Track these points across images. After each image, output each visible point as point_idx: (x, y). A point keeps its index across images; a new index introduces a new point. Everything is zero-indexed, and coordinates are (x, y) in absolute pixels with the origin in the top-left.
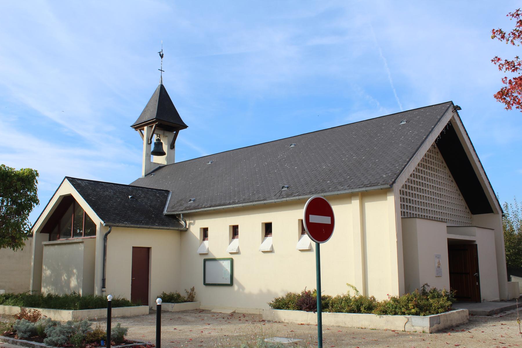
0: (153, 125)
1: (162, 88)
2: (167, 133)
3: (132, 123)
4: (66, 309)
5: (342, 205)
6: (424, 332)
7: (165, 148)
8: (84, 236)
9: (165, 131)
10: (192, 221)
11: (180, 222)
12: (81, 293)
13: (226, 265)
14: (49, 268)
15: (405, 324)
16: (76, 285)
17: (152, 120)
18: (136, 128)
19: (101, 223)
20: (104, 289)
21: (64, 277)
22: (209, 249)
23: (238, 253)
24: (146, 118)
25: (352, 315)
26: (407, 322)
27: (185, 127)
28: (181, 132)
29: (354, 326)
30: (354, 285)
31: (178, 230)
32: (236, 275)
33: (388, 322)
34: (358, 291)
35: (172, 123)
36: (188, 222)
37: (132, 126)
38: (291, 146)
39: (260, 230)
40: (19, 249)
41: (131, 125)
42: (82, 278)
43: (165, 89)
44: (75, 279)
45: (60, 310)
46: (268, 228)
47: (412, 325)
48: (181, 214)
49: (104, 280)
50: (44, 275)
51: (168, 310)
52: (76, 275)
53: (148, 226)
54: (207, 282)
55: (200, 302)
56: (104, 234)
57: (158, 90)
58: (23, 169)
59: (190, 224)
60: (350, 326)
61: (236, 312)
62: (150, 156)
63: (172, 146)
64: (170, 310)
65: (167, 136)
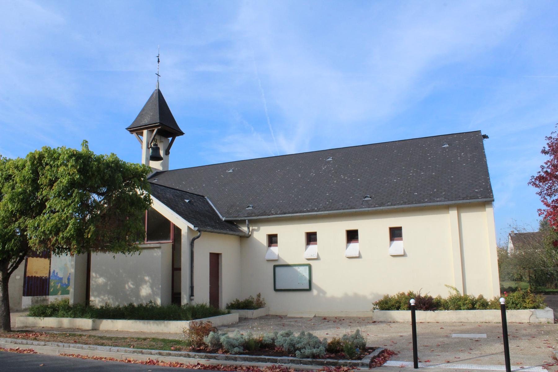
0: (154, 130)
1: (159, 93)
2: (163, 139)
3: (128, 125)
4: (172, 319)
5: (437, 214)
6: (548, 323)
7: (162, 153)
8: (147, 241)
9: (161, 137)
10: (256, 228)
11: (239, 228)
12: (159, 302)
13: (304, 271)
14: (101, 276)
15: (530, 316)
16: (150, 294)
17: (155, 124)
18: (132, 132)
19: (188, 227)
20: (192, 298)
21: (130, 285)
22: (279, 255)
23: (318, 259)
24: (146, 121)
25: (474, 312)
26: (532, 315)
27: (182, 133)
28: (177, 138)
29: (477, 321)
30: (454, 286)
31: (237, 235)
32: (314, 280)
33: (512, 315)
34: (458, 291)
35: (172, 129)
36: (251, 228)
37: (127, 129)
38: (328, 159)
39: (303, 239)
40: (129, 254)
41: (127, 127)
42: (160, 286)
43: (161, 94)
44: (147, 287)
45: (166, 322)
46: (352, 236)
47: (536, 317)
48: (247, 221)
49: (192, 288)
50: (94, 283)
51: (246, 317)
52: (150, 282)
53: (225, 232)
54: (278, 287)
55: (269, 308)
56: (191, 238)
57: (156, 94)
58: (122, 160)
59: (253, 230)
60: (473, 321)
61: (316, 315)
62: (149, 161)
63: (167, 153)
64: (249, 317)
65: (162, 142)
